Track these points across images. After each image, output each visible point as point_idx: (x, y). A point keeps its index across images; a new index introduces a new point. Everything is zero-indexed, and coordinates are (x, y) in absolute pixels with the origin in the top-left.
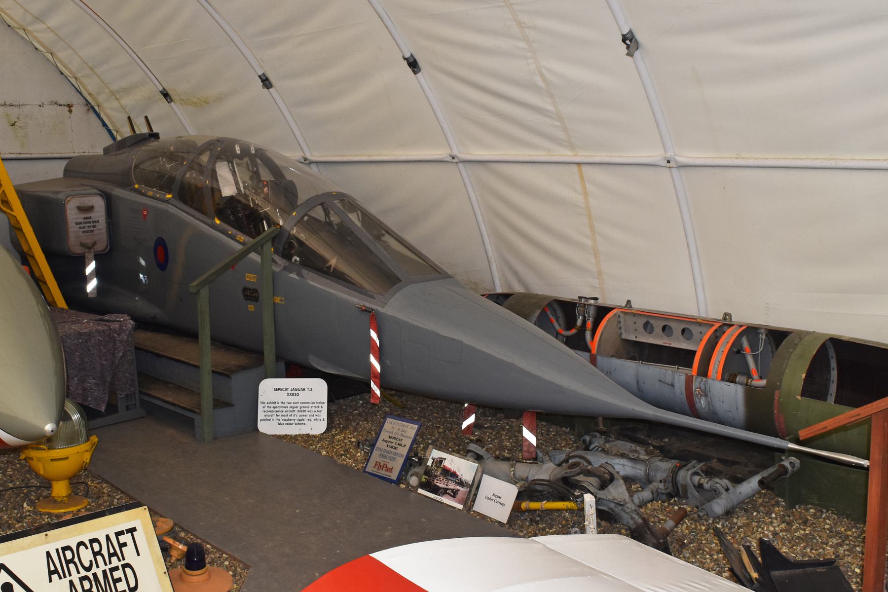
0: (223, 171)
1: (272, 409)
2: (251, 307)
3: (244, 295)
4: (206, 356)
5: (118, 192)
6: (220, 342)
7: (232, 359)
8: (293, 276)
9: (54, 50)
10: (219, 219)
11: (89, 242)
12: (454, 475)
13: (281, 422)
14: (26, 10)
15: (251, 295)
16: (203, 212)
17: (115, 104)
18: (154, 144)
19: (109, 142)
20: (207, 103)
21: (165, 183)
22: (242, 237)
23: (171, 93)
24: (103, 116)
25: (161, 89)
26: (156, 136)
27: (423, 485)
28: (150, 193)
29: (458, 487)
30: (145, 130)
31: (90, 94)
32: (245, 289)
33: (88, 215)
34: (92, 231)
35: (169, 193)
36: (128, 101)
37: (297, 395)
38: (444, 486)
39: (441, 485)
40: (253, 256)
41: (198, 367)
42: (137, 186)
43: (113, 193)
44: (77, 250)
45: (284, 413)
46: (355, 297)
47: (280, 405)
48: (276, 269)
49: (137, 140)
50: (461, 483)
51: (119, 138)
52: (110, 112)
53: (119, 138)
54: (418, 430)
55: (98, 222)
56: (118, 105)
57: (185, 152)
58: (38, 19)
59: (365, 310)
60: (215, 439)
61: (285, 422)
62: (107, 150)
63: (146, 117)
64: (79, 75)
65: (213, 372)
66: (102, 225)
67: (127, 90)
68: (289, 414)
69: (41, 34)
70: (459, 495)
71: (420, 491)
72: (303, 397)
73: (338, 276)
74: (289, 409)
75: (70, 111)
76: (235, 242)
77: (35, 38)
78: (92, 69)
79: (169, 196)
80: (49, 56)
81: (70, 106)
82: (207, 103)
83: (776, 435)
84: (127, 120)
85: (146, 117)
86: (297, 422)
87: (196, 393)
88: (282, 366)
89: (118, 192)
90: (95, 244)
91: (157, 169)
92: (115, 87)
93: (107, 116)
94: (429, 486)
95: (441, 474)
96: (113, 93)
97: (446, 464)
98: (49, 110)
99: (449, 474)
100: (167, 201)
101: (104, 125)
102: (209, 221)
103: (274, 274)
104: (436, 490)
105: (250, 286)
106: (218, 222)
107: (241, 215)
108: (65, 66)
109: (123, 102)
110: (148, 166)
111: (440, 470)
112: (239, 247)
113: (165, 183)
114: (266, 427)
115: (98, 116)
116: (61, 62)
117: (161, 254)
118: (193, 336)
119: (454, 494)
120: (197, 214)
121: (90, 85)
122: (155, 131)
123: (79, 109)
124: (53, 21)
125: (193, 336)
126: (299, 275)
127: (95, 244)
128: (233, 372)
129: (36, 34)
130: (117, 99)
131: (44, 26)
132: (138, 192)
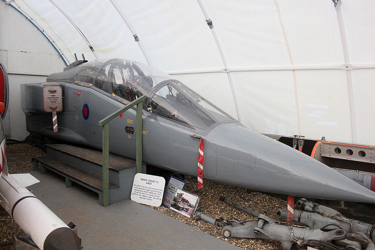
0: (117, 72)
1: (138, 189)
2: (129, 136)
3: (126, 130)
4: (106, 160)
6: (112, 154)
7: (117, 163)
8: (152, 120)
10: (115, 94)
11: (54, 107)
12: (187, 202)
13: (141, 196)
15: (129, 130)
19: (65, 66)
21: (90, 81)
22: (126, 101)
27: (173, 206)
29: (189, 208)
30: (82, 59)
32: (127, 127)
33: (54, 95)
34: (55, 102)
35: (91, 83)
37: (151, 184)
38: (183, 207)
39: (181, 206)
40: (130, 110)
41: (102, 166)
44: (48, 110)
45: (143, 193)
46: (169, 124)
47: (142, 188)
48: (144, 117)
50: (190, 206)
51: (68, 64)
54: (185, 185)
55: (58, 98)
59: (196, 138)
60: (109, 204)
61: (143, 197)
62: (65, 70)
65: (110, 169)
66: (60, 100)
68: (146, 193)
70: (189, 211)
71: (171, 208)
72: (154, 185)
73: (171, 117)
74: (146, 191)
76: (120, 103)
83: (114, 112)
84: (82, 55)
86: (148, 198)
87: (99, 178)
88: (145, 167)
89: (67, 85)
90: (56, 108)
91: (86, 75)
94: (175, 206)
95: (181, 201)
97: (184, 196)
99: (184, 200)
102: (109, 95)
103: (143, 119)
104: (178, 208)
105: (130, 126)
106: (114, 95)
107: (126, 93)
110: (82, 74)
111: (181, 199)
112: (123, 106)
113: (90, 81)
114: (133, 197)
117: (86, 112)
118: (100, 150)
119: (187, 210)
125: (100, 150)
126: (156, 119)
127: (56, 108)
128: (120, 170)
132: (77, 84)
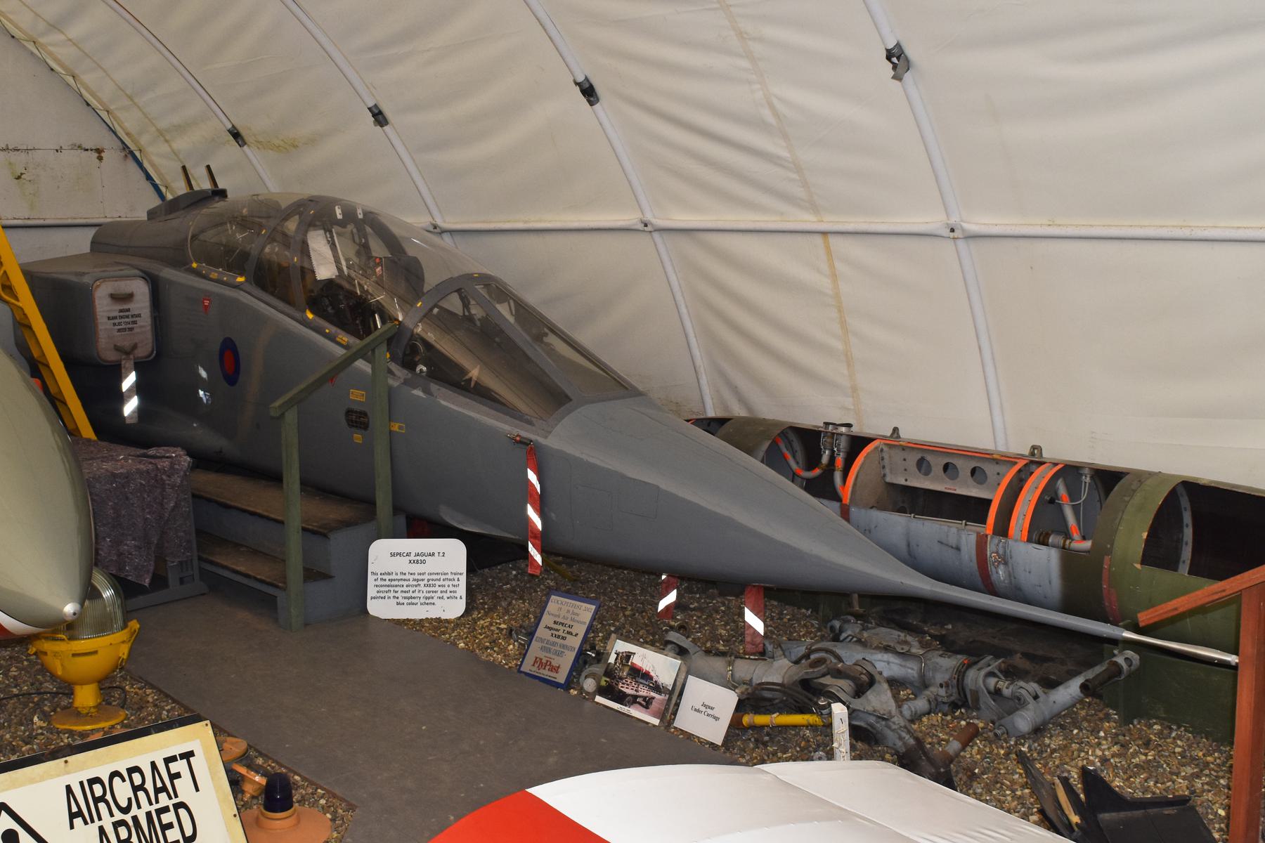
0: (318, 243)
1: (387, 583)
2: (358, 438)
3: (348, 420)
4: (294, 507)
5: (168, 273)
6: (314, 487)
7: (330, 512)
8: (418, 393)
9: (77, 72)
10: (312, 312)
11: (127, 344)
12: (647, 676)
13: (401, 600)
14: (37, 15)
15: (358, 419)
16: (289, 302)
17: (164, 148)
18: (219, 205)
19: (155, 202)
20: (295, 147)
21: (235, 260)
22: (344, 338)
23: (243, 132)
24: (146, 165)
25: (229, 126)
26: (222, 194)
27: (602, 691)
28: (214, 275)
29: (653, 694)
30: (207, 185)
31: (128, 134)
32: (349, 412)
33: (126, 307)
34: (131, 329)
35: (241, 275)
36: (182, 144)
37: (423, 562)
38: (633, 692)
39: (629, 691)
40: (361, 364)
41: (282, 522)
42: (194, 265)
43: (161, 274)
44: (110, 356)
45: (405, 589)
46: (506, 423)
47: (399, 577)
48: (393, 383)
49: (196, 200)
50: (657, 688)
51: (169, 197)
52: (156, 160)
53: (169, 197)
54: (596, 612)
55: (139, 316)
56: (168, 149)
57: (263, 217)
58: (54, 27)
59: (520, 442)
60: (306, 625)
61: (406, 601)
62: (152, 214)
63: (208, 167)
64: (112, 107)
65: (304, 529)
66: (146, 320)
67: (181, 129)
68: (412, 589)
69: (58, 48)
70: (655, 705)
71: (599, 699)
72: (432, 565)
73: (481, 393)
74: (411, 583)
75: (100, 158)
76: (334, 344)
77: (50, 54)
78: (130, 98)
79: (241, 279)
80: (70, 80)
81: (99, 151)
82: (295, 147)
83: (1105, 620)
84: (180, 170)
85: (208, 167)
86: (423, 601)
87: (279, 560)
88: (402, 521)
89: (168, 273)
90: (135, 347)
91: (224, 240)
92: (163, 124)
93: (153, 165)
94: (610, 692)
95: (629, 674)
96: (161, 133)
97: (636, 660)
98: (70, 157)
99: (639, 675)
100: (237, 287)
101: (149, 177)
102: (298, 315)
103: (390, 390)
104: (621, 698)
105: (356, 408)
106: (310, 316)
107: (343, 306)
108: (93, 94)
109: (175, 146)
110: (210, 236)
111: (626, 670)
112: (340, 352)
113: (235, 260)
114: (379, 607)
115: (140, 165)
116: (87, 89)
117: (230, 361)
118: (275, 478)
119: (647, 703)
120: (281, 305)
121: (128, 122)
122: (221, 186)
123: (112, 156)
124: (76, 30)
125: (275, 478)
126: (427, 391)
127: (135, 347)
128: (332, 530)
129: (51, 48)
130: (167, 141)
131: (62, 37)
132: (197, 273)
